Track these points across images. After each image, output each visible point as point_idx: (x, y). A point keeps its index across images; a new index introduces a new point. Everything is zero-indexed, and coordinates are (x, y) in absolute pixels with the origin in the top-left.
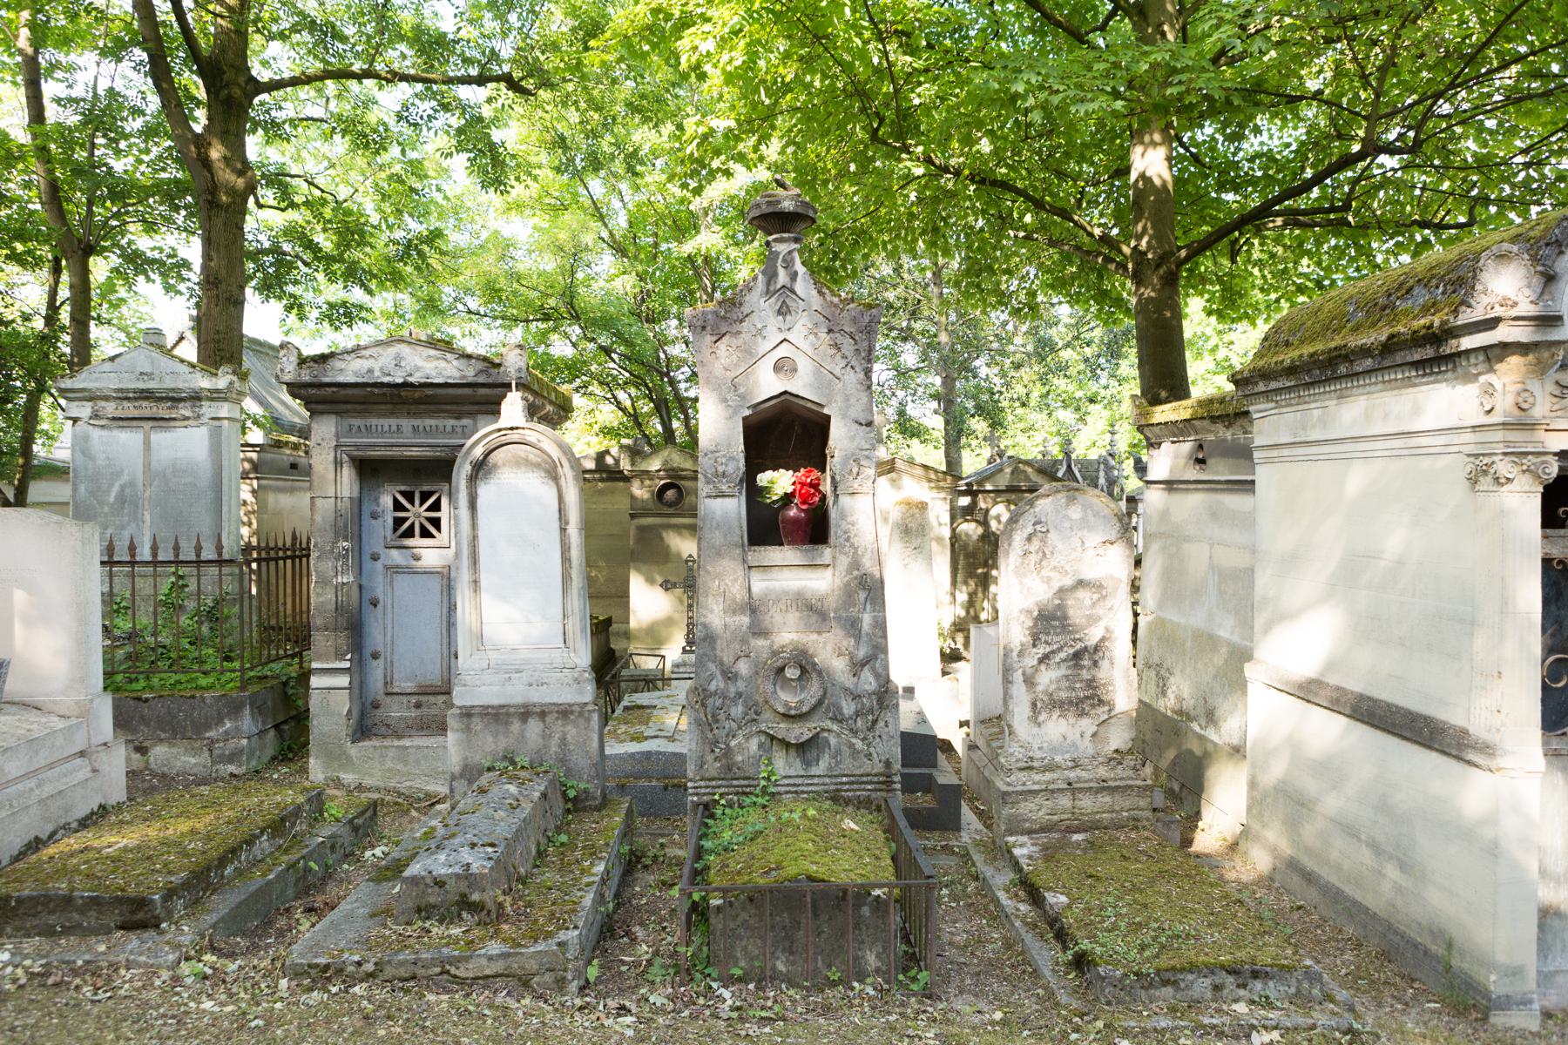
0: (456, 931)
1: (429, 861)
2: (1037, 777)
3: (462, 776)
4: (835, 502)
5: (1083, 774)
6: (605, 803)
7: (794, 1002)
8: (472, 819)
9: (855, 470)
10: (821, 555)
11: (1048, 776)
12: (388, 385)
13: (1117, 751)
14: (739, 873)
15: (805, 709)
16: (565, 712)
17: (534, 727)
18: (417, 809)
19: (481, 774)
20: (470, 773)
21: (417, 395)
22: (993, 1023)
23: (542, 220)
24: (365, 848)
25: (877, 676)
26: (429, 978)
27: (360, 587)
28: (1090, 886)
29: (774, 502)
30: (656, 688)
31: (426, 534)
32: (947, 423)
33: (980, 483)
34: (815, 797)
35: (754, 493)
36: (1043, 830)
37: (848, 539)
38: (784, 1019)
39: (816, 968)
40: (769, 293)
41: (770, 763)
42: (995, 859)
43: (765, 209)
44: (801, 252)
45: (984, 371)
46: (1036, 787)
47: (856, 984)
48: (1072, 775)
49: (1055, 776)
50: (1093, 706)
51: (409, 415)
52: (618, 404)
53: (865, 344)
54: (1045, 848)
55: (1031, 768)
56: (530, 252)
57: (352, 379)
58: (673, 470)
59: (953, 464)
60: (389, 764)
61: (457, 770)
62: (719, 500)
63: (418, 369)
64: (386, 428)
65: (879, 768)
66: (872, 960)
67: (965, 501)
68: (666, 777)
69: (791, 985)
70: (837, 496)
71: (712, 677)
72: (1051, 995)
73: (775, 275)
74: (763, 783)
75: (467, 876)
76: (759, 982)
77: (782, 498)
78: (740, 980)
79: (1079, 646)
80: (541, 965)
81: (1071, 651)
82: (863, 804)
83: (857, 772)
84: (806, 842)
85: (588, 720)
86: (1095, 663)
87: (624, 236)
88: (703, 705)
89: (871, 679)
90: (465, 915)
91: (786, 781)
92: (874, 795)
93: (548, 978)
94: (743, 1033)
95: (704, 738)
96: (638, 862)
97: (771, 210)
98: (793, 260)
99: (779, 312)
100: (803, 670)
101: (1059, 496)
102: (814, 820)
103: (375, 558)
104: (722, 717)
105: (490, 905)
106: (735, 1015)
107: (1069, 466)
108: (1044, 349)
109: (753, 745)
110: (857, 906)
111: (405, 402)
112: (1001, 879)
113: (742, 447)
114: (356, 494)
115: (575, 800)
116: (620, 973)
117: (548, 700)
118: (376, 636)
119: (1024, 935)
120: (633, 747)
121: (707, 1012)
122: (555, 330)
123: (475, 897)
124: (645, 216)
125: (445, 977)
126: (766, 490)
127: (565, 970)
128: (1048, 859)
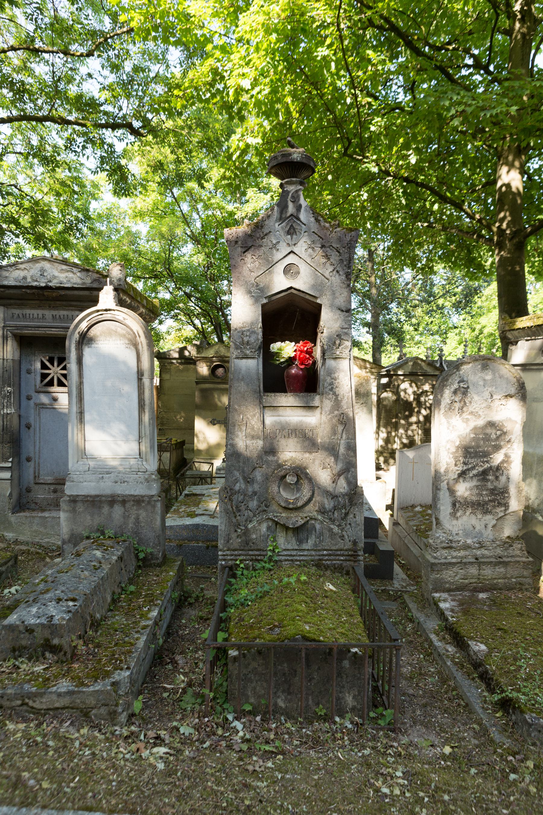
0: (39, 668)
1: (24, 613)
2: (455, 554)
3: (69, 541)
4: (324, 364)
5: (486, 552)
6: (165, 561)
7: (290, 733)
8: (64, 577)
9: (338, 342)
10: (313, 400)
11: (462, 553)
12: (36, 288)
13: (508, 537)
14: (251, 627)
15: (300, 504)
16: (138, 501)
17: (118, 510)
18: (50, 557)
19: (82, 539)
20: (75, 539)
21: (54, 295)
22: (444, 757)
23: (154, 222)
24: (5, 587)
25: (349, 483)
26: (12, 708)
27: (20, 416)
28: (501, 637)
29: (283, 363)
30: (206, 483)
31: (61, 384)
32: (374, 338)
33: (395, 370)
34: (305, 564)
35: (269, 357)
36: (457, 589)
37: (331, 389)
38: (283, 753)
39: (307, 706)
40: (281, 219)
41: (275, 540)
42: (424, 607)
43: (280, 160)
44: (304, 191)
45: (395, 310)
46: (454, 560)
47: (337, 719)
48: (479, 553)
49: (467, 553)
50: (494, 507)
51: (50, 308)
52: (194, 326)
53: (347, 256)
54: (461, 604)
55: (451, 548)
56: (148, 241)
57: (12, 283)
58: (221, 357)
59: (376, 362)
60: (35, 528)
61: (66, 537)
62: (244, 361)
63: (55, 277)
64: (36, 316)
65: (349, 545)
66: (349, 700)
67: (384, 381)
68: (208, 541)
69: (289, 717)
70: (324, 360)
71: (237, 481)
72: (485, 731)
73: (286, 206)
74: (270, 553)
75: (50, 626)
76: (264, 714)
77: (286, 361)
78: (250, 712)
79: (486, 466)
80: (98, 700)
81: (481, 469)
82: (338, 569)
83: (334, 548)
84: (300, 603)
85: (154, 507)
86: (497, 478)
87: (199, 233)
88: (230, 499)
89: (345, 485)
90: (47, 654)
91: (285, 553)
92: (345, 564)
93: (103, 711)
94: (250, 768)
95: (230, 521)
96: (186, 600)
97: (284, 160)
98: (298, 197)
99: (288, 233)
100: (299, 478)
101: (477, 363)
102: (305, 583)
103: (29, 398)
104: (243, 508)
105: (66, 648)
106: (245, 747)
107: (441, 364)
108: (429, 297)
109: (264, 528)
110: (340, 660)
111: (48, 299)
112: (432, 624)
113: (260, 325)
114: (17, 357)
115: (144, 560)
116: (162, 699)
117: (127, 493)
118: (29, 447)
119: (455, 673)
120: (189, 521)
121: (224, 743)
122: (160, 284)
123: (56, 641)
124: (210, 222)
125: (25, 708)
126: (277, 354)
127: (117, 705)
128: (466, 612)
